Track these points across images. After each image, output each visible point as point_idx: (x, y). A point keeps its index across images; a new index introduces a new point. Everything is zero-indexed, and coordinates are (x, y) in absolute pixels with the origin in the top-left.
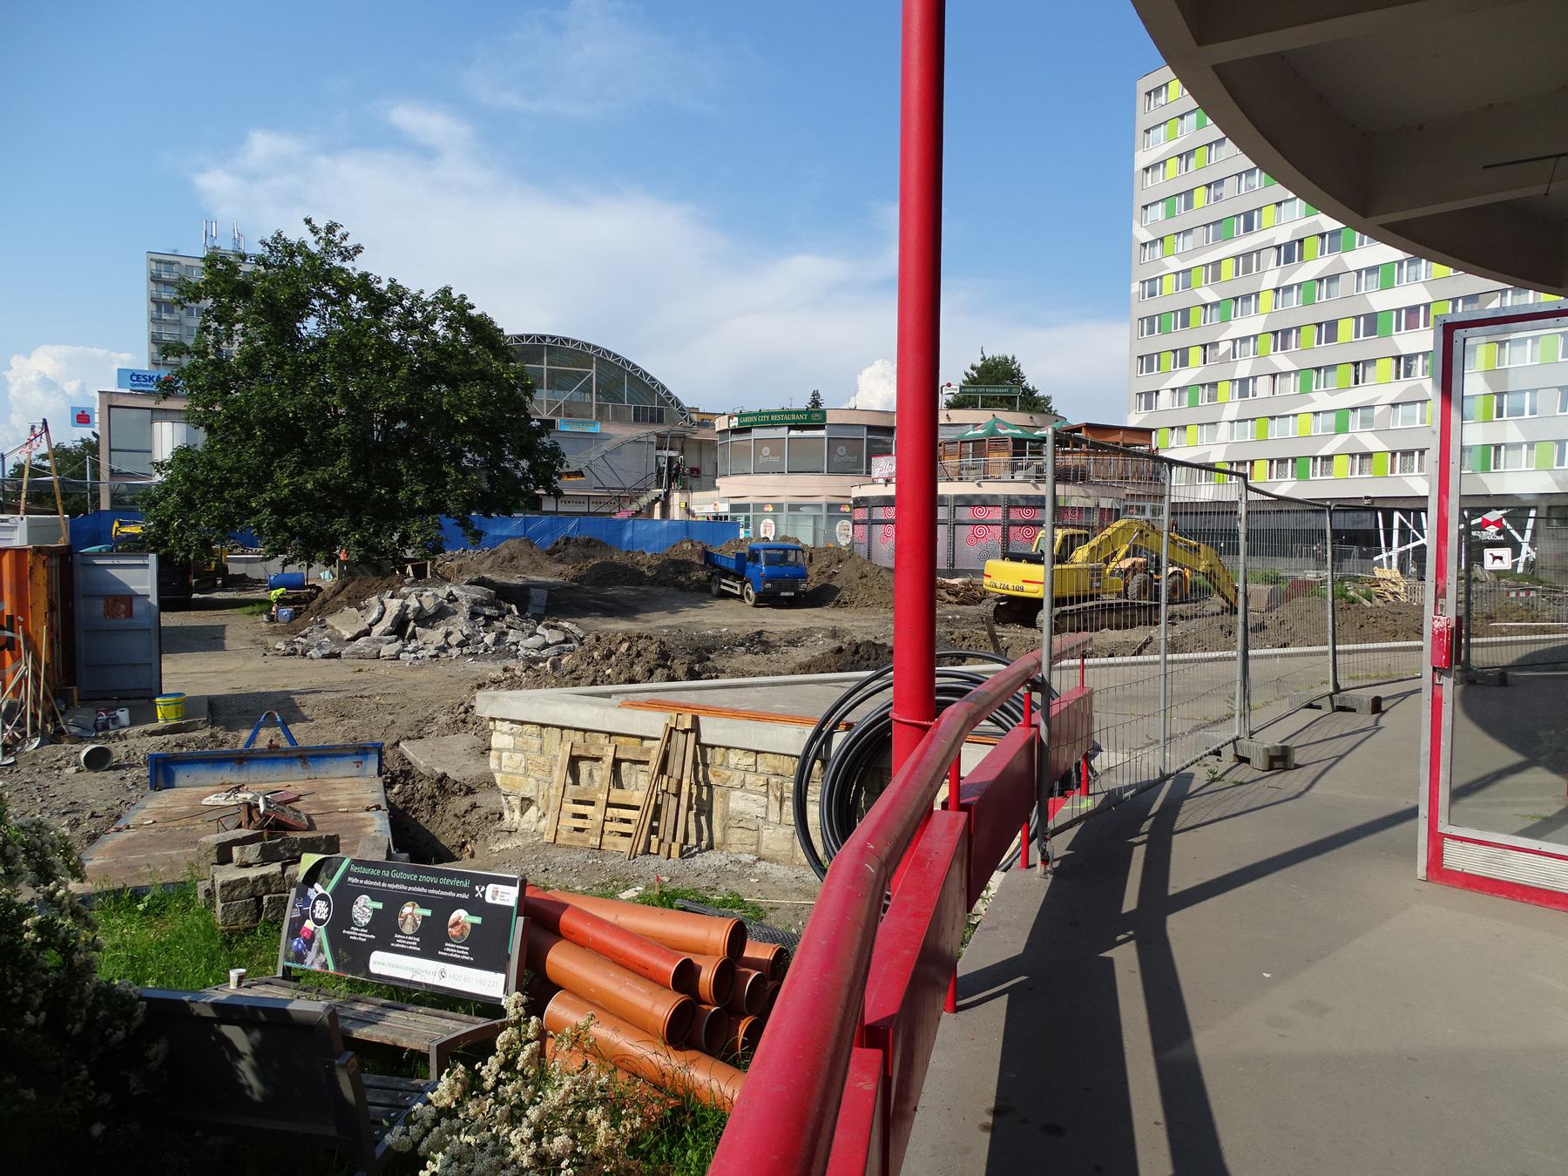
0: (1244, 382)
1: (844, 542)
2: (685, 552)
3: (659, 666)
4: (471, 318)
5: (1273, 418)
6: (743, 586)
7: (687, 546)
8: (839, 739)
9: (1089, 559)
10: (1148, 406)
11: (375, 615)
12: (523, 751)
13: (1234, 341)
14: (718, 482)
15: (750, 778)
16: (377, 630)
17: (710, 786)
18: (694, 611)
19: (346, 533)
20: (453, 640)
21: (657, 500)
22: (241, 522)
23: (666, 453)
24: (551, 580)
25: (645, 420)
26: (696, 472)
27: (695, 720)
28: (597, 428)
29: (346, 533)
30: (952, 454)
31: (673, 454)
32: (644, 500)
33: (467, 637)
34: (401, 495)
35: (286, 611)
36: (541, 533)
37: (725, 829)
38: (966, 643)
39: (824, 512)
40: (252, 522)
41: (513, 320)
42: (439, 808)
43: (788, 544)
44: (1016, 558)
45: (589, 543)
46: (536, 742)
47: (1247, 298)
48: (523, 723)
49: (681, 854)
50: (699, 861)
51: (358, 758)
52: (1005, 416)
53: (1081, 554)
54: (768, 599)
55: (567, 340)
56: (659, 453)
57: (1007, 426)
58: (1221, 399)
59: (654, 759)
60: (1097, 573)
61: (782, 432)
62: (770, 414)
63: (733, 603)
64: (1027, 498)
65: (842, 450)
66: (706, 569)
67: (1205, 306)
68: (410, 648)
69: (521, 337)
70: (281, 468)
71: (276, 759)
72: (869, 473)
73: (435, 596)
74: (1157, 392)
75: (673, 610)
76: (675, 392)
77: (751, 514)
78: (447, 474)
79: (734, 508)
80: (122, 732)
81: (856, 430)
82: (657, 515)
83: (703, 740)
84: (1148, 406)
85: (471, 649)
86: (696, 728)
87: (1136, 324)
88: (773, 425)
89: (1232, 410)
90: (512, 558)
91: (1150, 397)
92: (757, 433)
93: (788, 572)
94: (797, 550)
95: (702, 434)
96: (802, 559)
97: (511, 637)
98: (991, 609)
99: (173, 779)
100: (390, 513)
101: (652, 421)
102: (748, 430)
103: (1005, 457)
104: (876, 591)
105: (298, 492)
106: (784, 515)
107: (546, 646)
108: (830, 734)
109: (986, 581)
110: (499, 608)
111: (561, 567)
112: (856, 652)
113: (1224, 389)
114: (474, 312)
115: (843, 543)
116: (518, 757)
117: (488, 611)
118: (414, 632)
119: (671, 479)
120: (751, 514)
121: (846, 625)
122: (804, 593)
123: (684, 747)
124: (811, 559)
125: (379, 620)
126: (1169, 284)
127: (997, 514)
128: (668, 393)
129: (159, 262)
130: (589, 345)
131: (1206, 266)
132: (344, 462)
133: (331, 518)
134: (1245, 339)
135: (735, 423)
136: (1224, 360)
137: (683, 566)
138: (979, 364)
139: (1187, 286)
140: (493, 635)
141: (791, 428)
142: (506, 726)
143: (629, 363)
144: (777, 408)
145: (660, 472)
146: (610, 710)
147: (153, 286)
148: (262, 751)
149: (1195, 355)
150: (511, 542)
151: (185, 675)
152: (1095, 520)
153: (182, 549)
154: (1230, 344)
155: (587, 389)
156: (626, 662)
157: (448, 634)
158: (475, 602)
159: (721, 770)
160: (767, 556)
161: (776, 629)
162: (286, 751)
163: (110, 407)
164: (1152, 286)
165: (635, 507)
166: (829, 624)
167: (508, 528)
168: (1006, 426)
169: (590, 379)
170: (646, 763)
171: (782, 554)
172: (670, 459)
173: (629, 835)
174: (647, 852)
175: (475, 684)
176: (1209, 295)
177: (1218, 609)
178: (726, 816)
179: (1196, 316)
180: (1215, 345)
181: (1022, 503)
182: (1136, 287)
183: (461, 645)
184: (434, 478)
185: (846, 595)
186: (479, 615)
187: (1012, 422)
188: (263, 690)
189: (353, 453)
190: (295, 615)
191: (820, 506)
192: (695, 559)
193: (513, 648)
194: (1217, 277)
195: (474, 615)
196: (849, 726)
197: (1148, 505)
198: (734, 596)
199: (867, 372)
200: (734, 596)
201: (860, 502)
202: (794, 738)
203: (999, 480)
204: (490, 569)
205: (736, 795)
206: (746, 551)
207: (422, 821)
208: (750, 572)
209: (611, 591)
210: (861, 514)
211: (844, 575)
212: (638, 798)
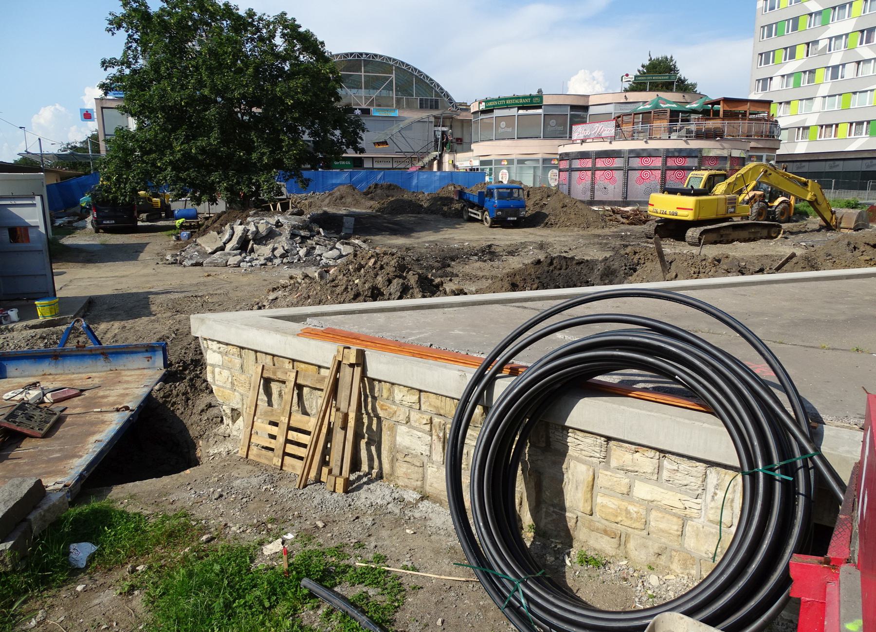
0: (835, 68)
1: (553, 184)
3: (396, 276)
4: (300, 34)
5: (855, 93)
6: (483, 213)
7: (451, 188)
8: (501, 386)
9: (726, 192)
10: (764, 89)
11: (227, 236)
12: (229, 369)
13: (830, 39)
14: (473, 146)
15: (415, 416)
16: (229, 246)
17: (379, 419)
18: (450, 231)
19: (219, 182)
20: (278, 253)
21: (435, 159)
22: (155, 177)
23: (441, 129)
24: (364, 211)
26: (460, 141)
27: (361, 354)
28: (396, 113)
29: (219, 182)
30: (627, 123)
31: (445, 129)
32: (426, 160)
33: (287, 251)
34: (254, 156)
35: (185, 234)
36: (360, 181)
37: (393, 460)
38: (637, 256)
39: (540, 165)
40: (160, 176)
41: (336, 44)
42: (190, 402)
45: (390, 187)
46: (237, 361)
47: (843, 7)
48: (227, 344)
49: (346, 491)
50: (363, 497)
51: (148, 355)
52: (664, 95)
53: (720, 188)
54: (499, 222)
55: (376, 55)
56: (436, 129)
57: (668, 102)
58: (817, 81)
59: (327, 385)
60: (732, 202)
61: (514, 111)
62: (506, 99)
64: (680, 150)
65: (553, 122)
66: (460, 203)
67: (811, 15)
68: (248, 259)
69: (347, 54)
70: (176, 139)
71: (83, 356)
72: (571, 137)
73: (268, 223)
74: (771, 78)
75: (437, 230)
76: (446, 88)
77: (493, 167)
78: (283, 141)
79: (482, 163)
80: (10, 326)
81: (563, 109)
82: (435, 168)
83: (370, 374)
84: (764, 89)
85: (289, 259)
86: (361, 360)
88: (508, 107)
90: (342, 198)
91: (765, 82)
92: (497, 113)
94: (519, 189)
95: (463, 116)
96: (523, 195)
97: (317, 251)
98: (653, 228)
99: (5, 371)
100: (247, 168)
101: (431, 108)
102: (491, 111)
103: (665, 123)
104: (573, 216)
105: (187, 155)
106: (514, 167)
107: (341, 256)
108: (493, 379)
109: (650, 208)
110: (311, 230)
111: (372, 203)
112: (551, 264)
113: (820, 74)
114: (301, 30)
115: (553, 185)
116: (226, 373)
117: (303, 233)
118: (252, 247)
119: (444, 145)
120: (493, 167)
121: (551, 240)
122: (523, 218)
123: (350, 379)
124: (528, 195)
125: (230, 240)
127: (658, 162)
128: (441, 89)
130: (390, 59)
132: (215, 134)
133: (209, 173)
135: (483, 106)
136: (822, 53)
137: (447, 201)
138: (647, 63)
140: (305, 249)
141: (519, 108)
142: (215, 346)
144: (511, 95)
145: (436, 141)
146: (290, 338)
148: (72, 350)
149: (801, 50)
150: (341, 187)
151: (76, 281)
153: (122, 195)
154: (827, 41)
155: (389, 88)
156: (372, 273)
157: (274, 249)
158: (294, 227)
159: (388, 404)
160: (499, 193)
161: (502, 243)
162: (91, 350)
163: (102, 108)
165: (421, 164)
166: (539, 239)
167: (340, 178)
169: (392, 81)
170: (322, 390)
171: (510, 192)
172: (443, 133)
173: (301, 458)
174: (318, 480)
175: (271, 287)
177: (817, 227)
178: (394, 449)
179: (803, 22)
180: (816, 42)
181: (676, 154)
183: (283, 256)
184: (275, 143)
185: (552, 218)
186: (296, 236)
187: (671, 99)
188: (134, 291)
189: (221, 128)
190: (190, 236)
191: (537, 160)
193: (318, 258)
195: (293, 236)
196: (514, 372)
197: (765, 155)
198: (476, 220)
199: (573, 79)
200: (476, 220)
201: (564, 157)
202: (454, 380)
204: (328, 205)
205: (402, 429)
206: (484, 190)
207: (178, 413)
208: (487, 204)
209: (400, 218)
210: (564, 165)
211: (551, 206)
212: (311, 424)
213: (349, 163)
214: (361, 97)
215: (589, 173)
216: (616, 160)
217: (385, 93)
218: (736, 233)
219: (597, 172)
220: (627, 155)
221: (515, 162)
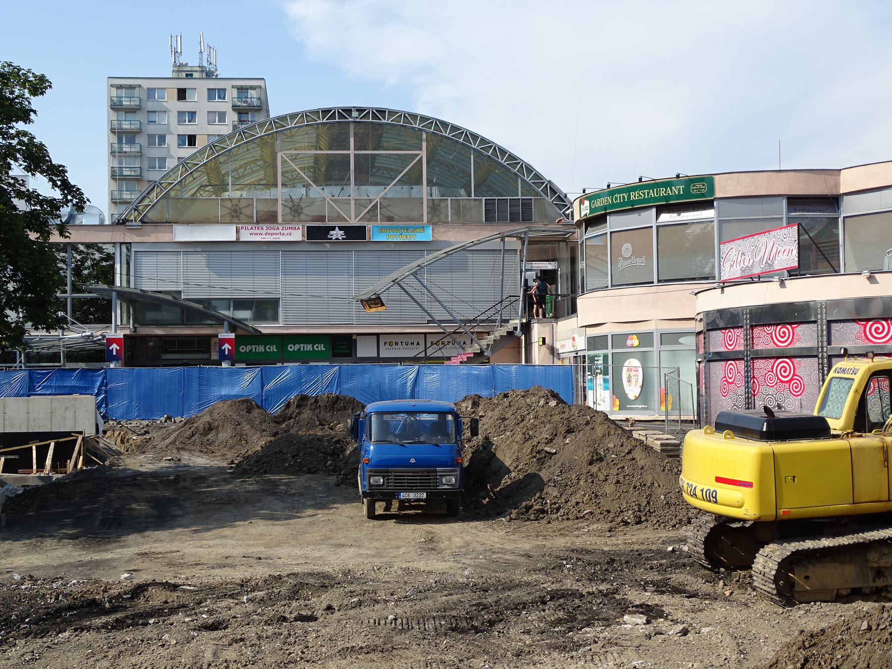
25: (502, 219)
28: (427, 235)
55: (382, 112)
61: (649, 218)
76: (547, 175)
88: (634, 208)
92: (614, 223)
101: (514, 219)
104: (609, 488)
128: (538, 176)
129: (120, 87)
141: (660, 210)
147: (114, 116)
155: (413, 179)
160: (385, 427)
169: (421, 159)
213: (274, 349)
214: (348, 202)
215: (741, 365)
216: (801, 329)
217: (403, 192)
219: (759, 364)
220: (747, 322)
221: (656, 339)
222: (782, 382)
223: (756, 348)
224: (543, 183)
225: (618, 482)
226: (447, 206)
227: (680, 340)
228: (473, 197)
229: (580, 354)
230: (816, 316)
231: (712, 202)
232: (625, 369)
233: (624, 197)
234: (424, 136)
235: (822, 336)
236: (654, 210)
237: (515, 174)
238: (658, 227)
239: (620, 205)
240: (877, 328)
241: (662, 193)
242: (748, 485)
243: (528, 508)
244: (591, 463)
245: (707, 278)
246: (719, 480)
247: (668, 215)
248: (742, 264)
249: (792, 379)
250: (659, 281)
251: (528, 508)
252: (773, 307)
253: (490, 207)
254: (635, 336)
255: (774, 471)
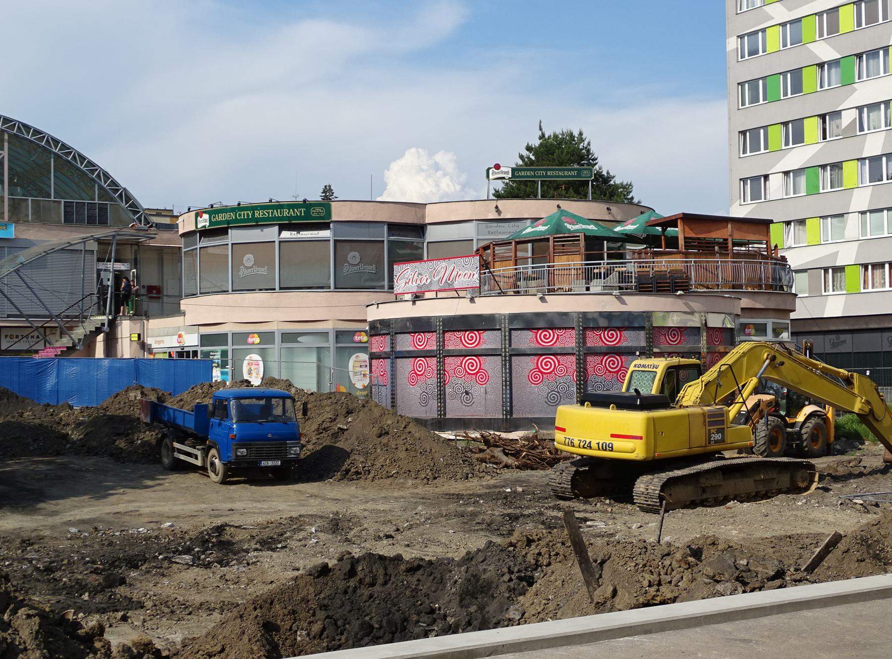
0: (875, 160)
2: (132, 404)
6: (206, 452)
9: (703, 401)
10: (756, 196)
13: (860, 109)
14: (185, 304)
21: (98, 331)
23: (110, 266)
25: (80, 221)
26: (155, 292)
30: (504, 260)
32: (79, 332)
39: (331, 342)
43: (275, 389)
44: (601, 402)
47: (873, 54)
53: (691, 393)
54: (244, 472)
56: (102, 266)
58: (847, 184)
60: (717, 421)
61: (271, 233)
62: (253, 208)
63: (193, 478)
64: (609, 316)
65: (353, 256)
67: (821, 65)
72: (391, 287)
74: (766, 177)
75: (100, 492)
76: (123, 183)
77: (229, 348)
79: (205, 340)
82: (100, 351)
84: (756, 196)
87: (734, 90)
88: (258, 224)
89: (862, 199)
91: (756, 183)
92: (235, 236)
93: (269, 430)
94: (284, 398)
95: (162, 239)
96: (294, 412)
98: (567, 477)
101: (91, 222)
102: (223, 232)
103: (577, 262)
104: (402, 454)
106: (275, 349)
112: (352, 573)
115: (359, 385)
120: (229, 348)
121: (356, 509)
122: (297, 460)
126: (774, 40)
127: (569, 340)
128: (114, 183)
131: (820, 14)
134: (873, 107)
135: (204, 222)
136: (848, 134)
137: (122, 425)
138: (536, 143)
139: (797, 40)
141: (282, 227)
143: (56, 142)
144: (264, 199)
145: (102, 290)
149: (812, 128)
152: (703, 344)
154: (854, 113)
160: (241, 409)
161: (248, 521)
164: (752, 43)
165: (66, 342)
166: (330, 508)
168: (576, 219)
171: (266, 408)
172: (119, 276)
176: (825, 51)
179: (810, 78)
180: (837, 114)
181: (603, 323)
182: (732, 43)
187: (584, 215)
191: (325, 334)
192: (137, 413)
194: (834, 28)
197: (770, 323)
198: (193, 468)
199: (395, 166)
200: (193, 468)
201: (378, 328)
203: (569, 292)
206: (208, 401)
210: (380, 344)
216: (486, 335)
218: (732, 482)
219: (449, 360)
220: (506, 325)
221: (278, 338)
222: (469, 374)
223: (446, 348)
224: (118, 190)
225: (407, 450)
226: (27, 206)
227: (299, 339)
228: (52, 199)
229: (186, 349)
230: (500, 325)
231: (329, 224)
232: (245, 363)
233: (248, 215)
234: (6, 137)
235: (505, 340)
236: (277, 228)
237: (93, 180)
238: (280, 242)
239: (244, 221)
240: (545, 335)
241: (286, 214)
242: (641, 438)
243: (348, 471)
244: (380, 436)
245: (322, 288)
246: (613, 436)
247: (289, 233)
248: (418, 282)
249: (478, 372)
250: (281, 288)
251: (348, 471)
252: (463, 317)
253: (69, 209)
254: (256, 335)
255: (654, 428)
